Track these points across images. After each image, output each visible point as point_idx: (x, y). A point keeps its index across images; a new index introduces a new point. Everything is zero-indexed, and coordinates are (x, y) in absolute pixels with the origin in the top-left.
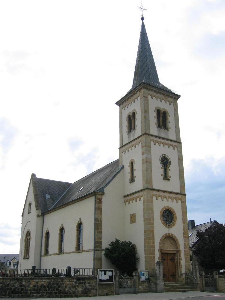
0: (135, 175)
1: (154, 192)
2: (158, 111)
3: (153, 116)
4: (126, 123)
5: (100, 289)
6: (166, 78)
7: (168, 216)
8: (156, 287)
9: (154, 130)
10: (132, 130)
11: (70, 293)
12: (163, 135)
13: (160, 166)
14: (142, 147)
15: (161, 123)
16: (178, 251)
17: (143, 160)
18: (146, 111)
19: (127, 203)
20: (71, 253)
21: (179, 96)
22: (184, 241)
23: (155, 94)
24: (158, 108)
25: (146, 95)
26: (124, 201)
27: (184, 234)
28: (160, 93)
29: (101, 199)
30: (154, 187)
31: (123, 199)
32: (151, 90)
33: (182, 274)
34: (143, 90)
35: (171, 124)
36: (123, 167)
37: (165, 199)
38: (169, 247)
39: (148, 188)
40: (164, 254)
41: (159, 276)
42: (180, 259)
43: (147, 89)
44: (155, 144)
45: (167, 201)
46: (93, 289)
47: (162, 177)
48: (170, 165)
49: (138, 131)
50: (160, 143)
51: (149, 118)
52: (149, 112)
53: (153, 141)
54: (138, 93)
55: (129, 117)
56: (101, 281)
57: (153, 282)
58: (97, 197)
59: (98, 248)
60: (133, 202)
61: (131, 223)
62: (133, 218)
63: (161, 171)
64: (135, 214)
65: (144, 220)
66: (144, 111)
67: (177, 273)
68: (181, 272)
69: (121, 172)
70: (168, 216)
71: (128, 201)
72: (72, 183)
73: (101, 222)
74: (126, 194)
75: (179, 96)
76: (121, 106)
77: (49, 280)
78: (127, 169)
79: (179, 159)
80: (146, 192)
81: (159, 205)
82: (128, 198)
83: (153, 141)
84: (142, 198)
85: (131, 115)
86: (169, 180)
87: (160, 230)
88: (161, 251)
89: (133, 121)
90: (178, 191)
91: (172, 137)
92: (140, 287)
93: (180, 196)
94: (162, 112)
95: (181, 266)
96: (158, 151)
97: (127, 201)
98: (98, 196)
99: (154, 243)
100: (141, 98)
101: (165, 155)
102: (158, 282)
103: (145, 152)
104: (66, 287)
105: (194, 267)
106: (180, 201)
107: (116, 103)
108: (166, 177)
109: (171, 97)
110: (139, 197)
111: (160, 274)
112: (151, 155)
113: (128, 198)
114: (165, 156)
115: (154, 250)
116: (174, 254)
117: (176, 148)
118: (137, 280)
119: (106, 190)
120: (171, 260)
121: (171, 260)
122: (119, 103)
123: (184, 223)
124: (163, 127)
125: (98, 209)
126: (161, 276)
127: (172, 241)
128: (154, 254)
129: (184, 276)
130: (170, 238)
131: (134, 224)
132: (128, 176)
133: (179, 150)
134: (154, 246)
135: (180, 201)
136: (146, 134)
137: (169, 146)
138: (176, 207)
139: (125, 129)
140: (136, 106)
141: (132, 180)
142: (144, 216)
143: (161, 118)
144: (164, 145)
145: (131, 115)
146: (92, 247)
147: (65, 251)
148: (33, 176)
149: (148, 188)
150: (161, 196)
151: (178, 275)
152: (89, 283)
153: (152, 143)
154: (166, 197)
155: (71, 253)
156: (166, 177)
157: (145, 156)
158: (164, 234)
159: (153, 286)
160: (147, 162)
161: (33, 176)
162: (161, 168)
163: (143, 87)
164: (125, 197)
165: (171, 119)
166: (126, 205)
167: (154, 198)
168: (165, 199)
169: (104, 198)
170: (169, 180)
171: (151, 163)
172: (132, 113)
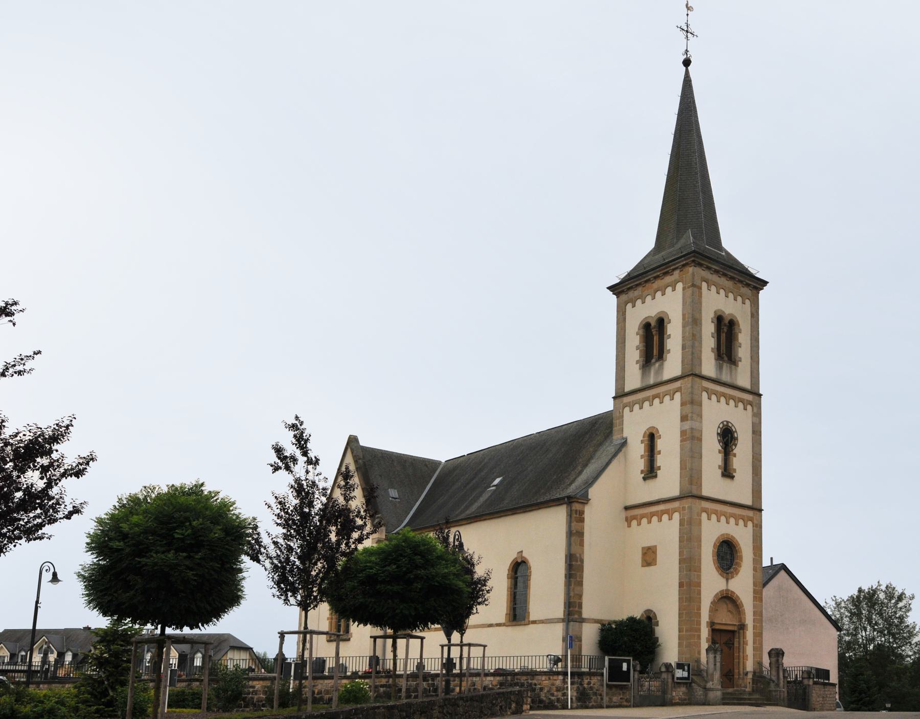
0: (660, 461)
1: (705, 504)
2: (719, 319)
3: (708, 328)
4: (634, 341)
5: (607, 694)
6: (737, 239)
7: (727, 555)
8: (706, 695)
9: (709, 367)
10: (653, 360)
11: (551, 702)
12: (725, 377)
13: (718, 446)
14: (683, 404)
15: (723, 348)
16: (742, 627)
17: (683, 433)
18: (692, 321)
19: (634, 523)
20: (491, 625)
21: (765, 283)
22: (754, 606)
23: (715, 278)
24: (719, 314)
25: (697, 282)
26: (627, 519)
27: (755, 592)
28: (725, 275)
29: (582, 513)
30: (705, 493)
31: (623, 514)
32: (709, 268)
33: (747, 674)
34: (691, 269)
35: (743, 352)
36: (624, 443)
37: (723, 519)
38: (726, 619)
39: (691, 494)
40: (716, 632)
41: (713, 674)
42: (745, 643)
43: (700, 265)
44: (710, 398)
45: (728, 522)
46: (595, 694)
47: (719, 472)
48: (736, 445)
49: (673, 365)
50: (719, 395)
51: (701, 337)
52: (701, 324)
53: (706, 390)
54: (677, 273)
55: (646, 327)
56: (678, 678)
57: (699, 686)
58: (574, 508)
59: (576, 616)
60: (639, 524)
61: (643, 566)
62: (649, 556)
63: (719, 459)
64: (656, 547)
65: (681, 561)
66: (690, 320)
67: (736, 671)
68: (744, 668)
69: (620, 455)
70: (727, 555)
71: (639, 519)
72: (440, 463)
73: (582, 561)
74: (629, 503)
75: (765, 283)
76: (624, 297)
77: (768, 665)
78: (636, 449)
79: (754, 432)
80: (687, 503)
81: (712, 531)
82: (634, 512)
83: (706, 390)
84: (676, 516)
85: (653, 324)
86: (732, 477)
87: (712, 582)
88: (711, 624)
89: (656, 338)
90: (748, 501)
91: (743, 380)
92: (674, 694)
93: (750, 513)
94: (727, 322)
95: (745, 657)
96: (716, 412)
97: (634, 518)
98: (576, 506)
99: (699, 608)
100: (684, 289)
101: (728, 422)
102: (710, 685)
103: (690, 415)
104: (541, 689)
105: (774, 660)
106: (750, 524)
107: (610, 288)
108: (727, 472)
109: (748, 285)
110: (670, 513)
111: (715, 669)
112: (701, 422)
113: (634, 512)
114: (727, 425)
115: (699, 623)
116: (733, 632)
117: (749, 407)
118: (670, 680)
119: (593, 492)
120: (726, 644)
121: (726, 644)
122: (621, 288)
123: (755, 569)
124: (726, 358)
125: (575, 535)
126: (717, 675)
127: (730, 606)
128: (699, 630)
129: (750, 676)
130: (728, 599)
131: (652, 568)
132: (640, 464)
133: (755, 410)
134: (699, 615)
135: (750, 524)
136: (691, 373)
137: (738, 401)
138: (742, 535)
139: (634, 354)
140: (669, 302)
141: (651, 472)
142: (681, 553)
143: (723, 336)
144: (728, 398)
145: (653, 324)
146: (559, 611)
147: (532, 618)
148: (352, 442)
149: (691, 494)
150: (715, 512)
151: (739, 674)
152: (589, 683)
153: (705, 394)
154: (724, 514)
155: (491, 625)
156: (727, 472)
157: (687, 425)
158: (717, 591)
159: (699, 692)
160: (691, 439)
161: (352, 442)
162: (720, 452)
163: (693, 261)
164: (627, 508)
165: (743, 338)
166: (629, 526)
167: (704, 515)
168: (723, 519)
169: (589, 512)
170: (732, 477)
171: (700, 440)
172: (655, 319)
